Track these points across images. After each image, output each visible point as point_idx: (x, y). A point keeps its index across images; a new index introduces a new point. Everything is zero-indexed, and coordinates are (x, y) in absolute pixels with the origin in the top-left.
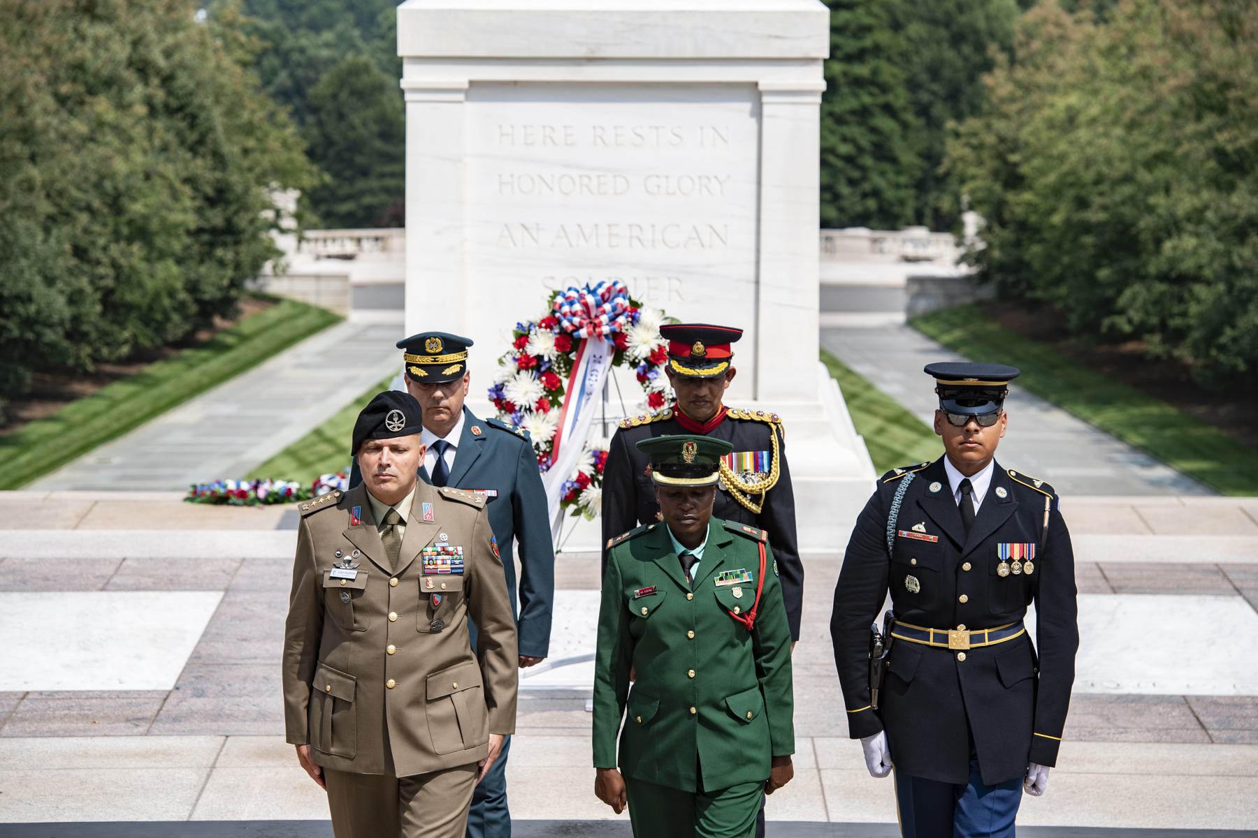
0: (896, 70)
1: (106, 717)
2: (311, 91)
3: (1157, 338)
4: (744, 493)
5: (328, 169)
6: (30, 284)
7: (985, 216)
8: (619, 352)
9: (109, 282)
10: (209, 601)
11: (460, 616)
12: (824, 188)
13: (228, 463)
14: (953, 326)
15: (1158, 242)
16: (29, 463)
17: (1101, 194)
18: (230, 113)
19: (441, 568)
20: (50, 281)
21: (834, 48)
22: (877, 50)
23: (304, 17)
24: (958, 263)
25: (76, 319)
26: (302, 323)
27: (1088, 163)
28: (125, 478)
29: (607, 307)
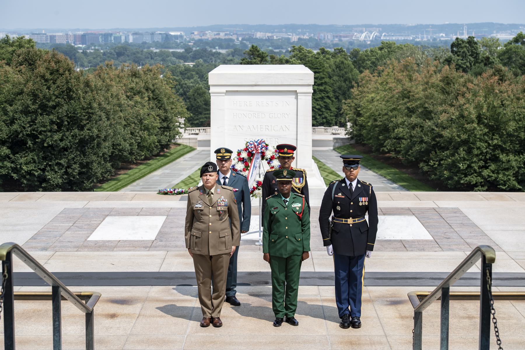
0: (330, 88)
1: (139, 246)
2: (188, 94)
4: (296, 188)
5: (192, 113)
6: (120, 141)
7: (353, 123)
8: (263, 157)
9: (139, 141)
10: (163, 219)
11: (227, 217)
12: (313, 117)
13: (168, 184)
14: (345, 150)
15: (394, 130)
16: (120, 185)
17: (380, 118)
19: (222, 204)
20: (125, 140)
21: (315, 82)
22: (326, 83)
23: (186, 76)
24: (346, 135)
25: (131, 149)
26: (186, 150)
27: (377, 110)
28: (143, 188)
29: (260, 146)
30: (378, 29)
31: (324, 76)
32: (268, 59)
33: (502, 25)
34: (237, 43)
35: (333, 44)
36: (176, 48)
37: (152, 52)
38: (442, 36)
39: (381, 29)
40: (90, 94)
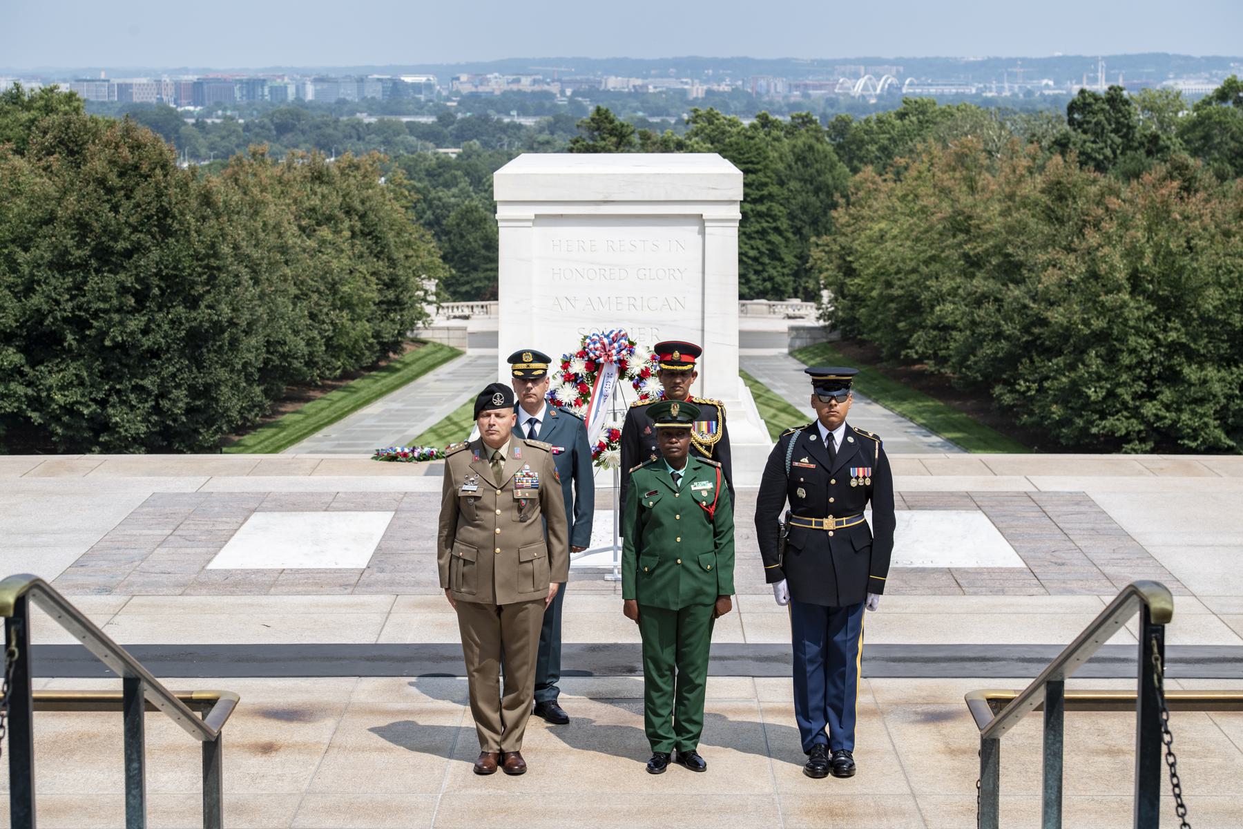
0: (781, 208)
1: (328, 584)
2: (444, 222)
3: (931, 362)
4: (701, 445)
5: (454, 267)
7: (835, 292)
8: (622, 372)
9: (330, 333)
10: (385, 518)
11: (536, 514)
12: (741, 276)
13: (398, 436)
14: (816, 355)
15: (932, 307)
16: (284, 438)
17: (900, 279)
18: (398, 234)
19: (526, 484)
20: (296, 333)
21: (746, 195)
22: (771, 197)
23: (441, 180)
24: (818, 319)
25: (311, 354)
26: (439, 355)
27: (892, 262)
28: (339, 445)
29: (616, 345)
30: (894, 69)
31: (767, 180)
32: (635, 139)
33: (1187, 58)
34: (562, 101)
35: (788, 105)
36: (416, 114)
37: (360, 123)
38: (1047, 86)
39: (901, 69)
40: (213, 222)
